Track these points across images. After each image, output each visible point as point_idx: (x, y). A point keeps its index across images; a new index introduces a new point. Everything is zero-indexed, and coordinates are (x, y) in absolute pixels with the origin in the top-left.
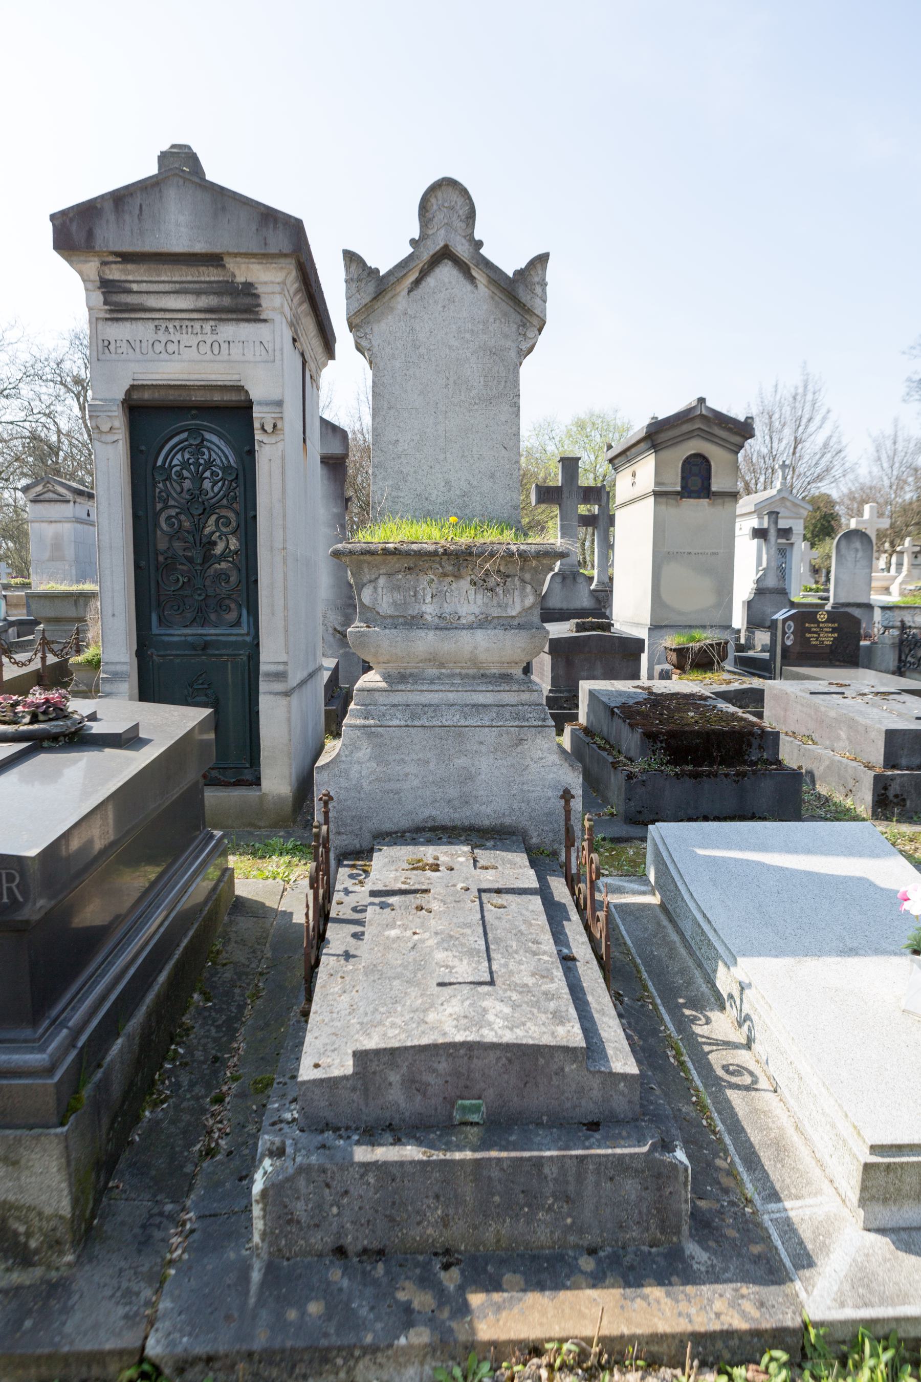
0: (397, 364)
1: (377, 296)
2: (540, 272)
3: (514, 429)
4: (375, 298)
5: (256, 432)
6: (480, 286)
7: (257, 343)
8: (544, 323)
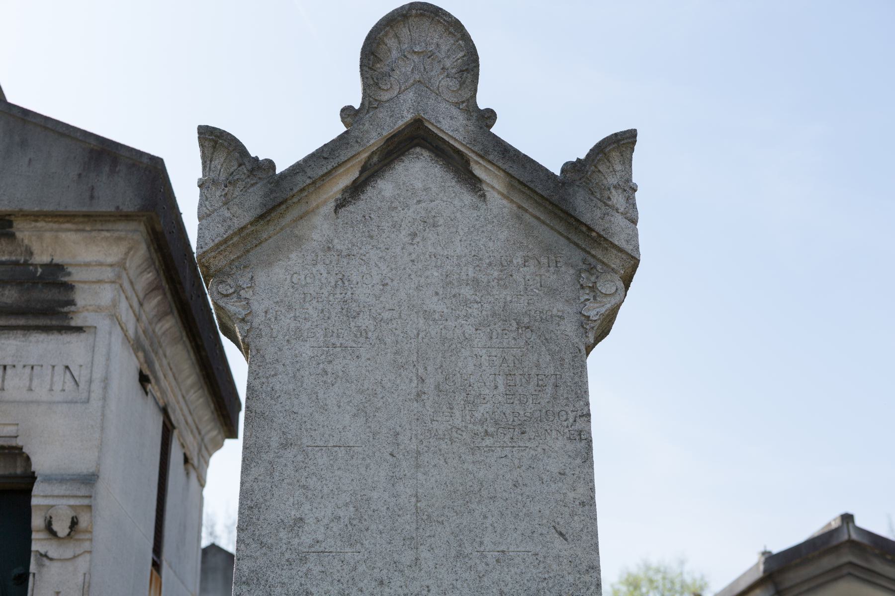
0: (306, 350)
1: (267, 214)
2: (618, 167)
3: (581, 489)
4: (261, 217)
5: (34, 536)
6: (491, 195)
7: (60, 369)
8: (634, 263)
